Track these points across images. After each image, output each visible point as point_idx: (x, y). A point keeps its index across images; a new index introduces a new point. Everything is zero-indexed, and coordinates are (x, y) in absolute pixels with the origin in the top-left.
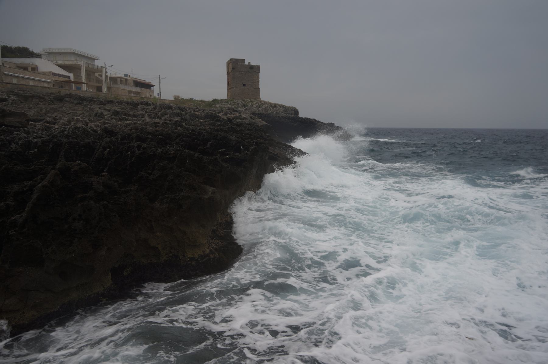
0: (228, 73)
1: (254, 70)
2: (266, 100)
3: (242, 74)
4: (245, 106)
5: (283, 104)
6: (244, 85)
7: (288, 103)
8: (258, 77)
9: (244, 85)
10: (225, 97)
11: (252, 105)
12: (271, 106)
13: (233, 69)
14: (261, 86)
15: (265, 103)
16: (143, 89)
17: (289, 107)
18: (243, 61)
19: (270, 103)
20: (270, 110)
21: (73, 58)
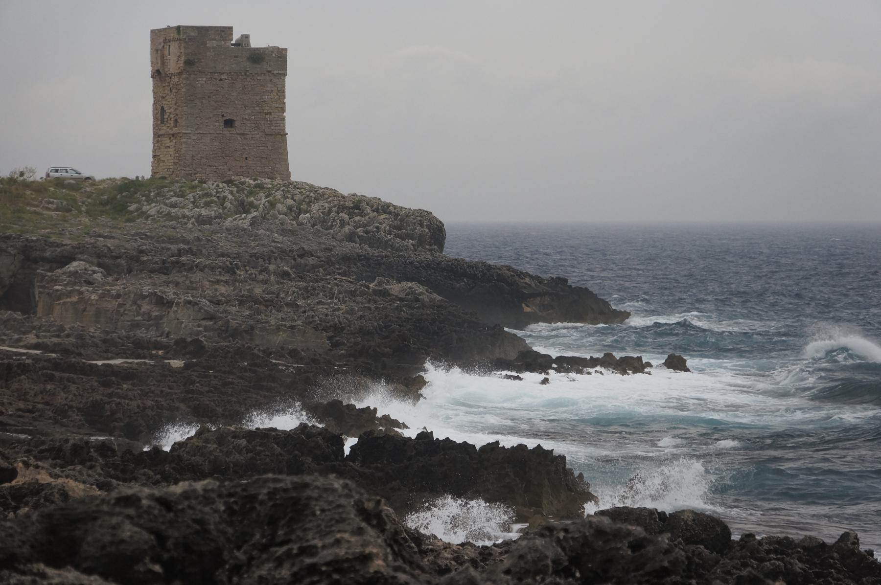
0: (157, 75)
1: (269, 64)
2: (320, 182)
3: (217, 85)
4: (243, 208)
5: (386, 199)
6: (229, 123)
7: (406, 199)
8: (282, 93)
9: (229, 123)
10: (140, 167)
11: (272, 205)
12: (342, 208)
13: (189, 63)
14: (290, 127)
15: (317, 194)
16: (622, 505)
17: (410, 213)
18: (227, 31)
19: (335, 194)
20: (343, 224)
21: (848, 446)
